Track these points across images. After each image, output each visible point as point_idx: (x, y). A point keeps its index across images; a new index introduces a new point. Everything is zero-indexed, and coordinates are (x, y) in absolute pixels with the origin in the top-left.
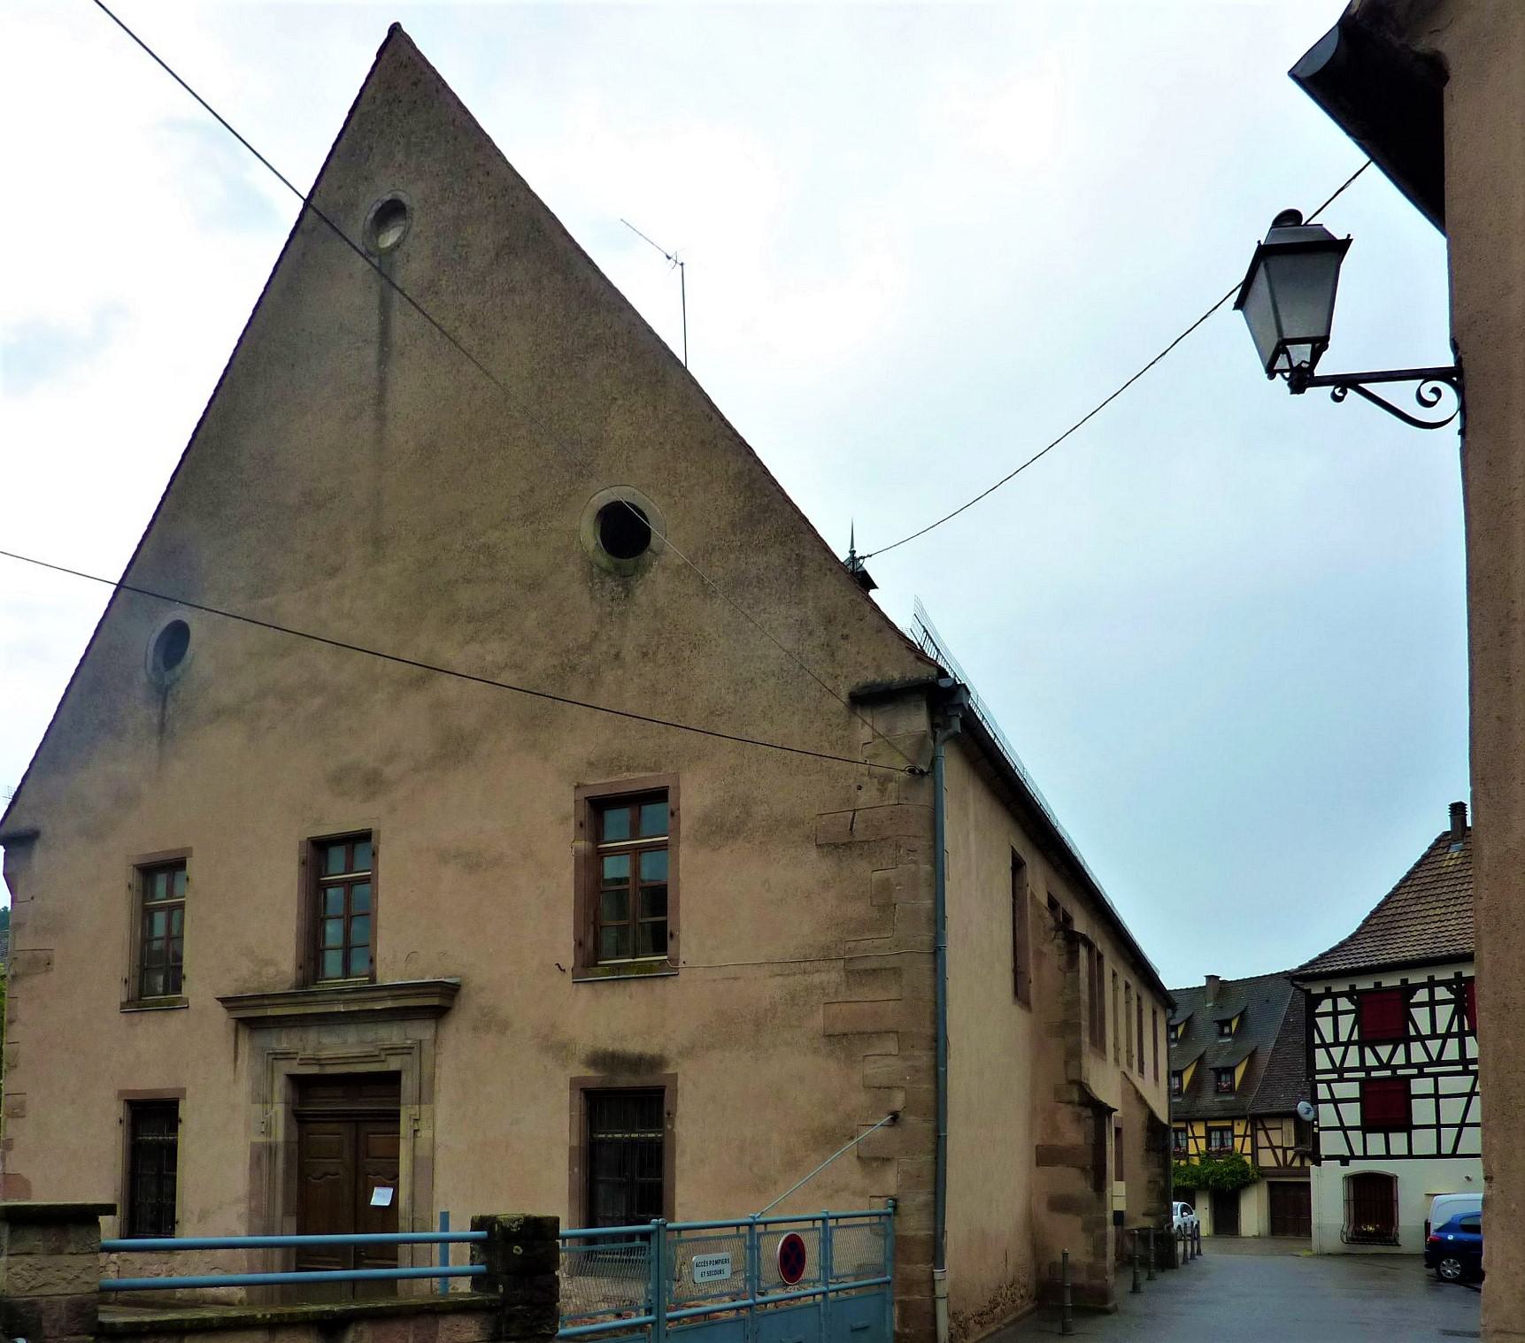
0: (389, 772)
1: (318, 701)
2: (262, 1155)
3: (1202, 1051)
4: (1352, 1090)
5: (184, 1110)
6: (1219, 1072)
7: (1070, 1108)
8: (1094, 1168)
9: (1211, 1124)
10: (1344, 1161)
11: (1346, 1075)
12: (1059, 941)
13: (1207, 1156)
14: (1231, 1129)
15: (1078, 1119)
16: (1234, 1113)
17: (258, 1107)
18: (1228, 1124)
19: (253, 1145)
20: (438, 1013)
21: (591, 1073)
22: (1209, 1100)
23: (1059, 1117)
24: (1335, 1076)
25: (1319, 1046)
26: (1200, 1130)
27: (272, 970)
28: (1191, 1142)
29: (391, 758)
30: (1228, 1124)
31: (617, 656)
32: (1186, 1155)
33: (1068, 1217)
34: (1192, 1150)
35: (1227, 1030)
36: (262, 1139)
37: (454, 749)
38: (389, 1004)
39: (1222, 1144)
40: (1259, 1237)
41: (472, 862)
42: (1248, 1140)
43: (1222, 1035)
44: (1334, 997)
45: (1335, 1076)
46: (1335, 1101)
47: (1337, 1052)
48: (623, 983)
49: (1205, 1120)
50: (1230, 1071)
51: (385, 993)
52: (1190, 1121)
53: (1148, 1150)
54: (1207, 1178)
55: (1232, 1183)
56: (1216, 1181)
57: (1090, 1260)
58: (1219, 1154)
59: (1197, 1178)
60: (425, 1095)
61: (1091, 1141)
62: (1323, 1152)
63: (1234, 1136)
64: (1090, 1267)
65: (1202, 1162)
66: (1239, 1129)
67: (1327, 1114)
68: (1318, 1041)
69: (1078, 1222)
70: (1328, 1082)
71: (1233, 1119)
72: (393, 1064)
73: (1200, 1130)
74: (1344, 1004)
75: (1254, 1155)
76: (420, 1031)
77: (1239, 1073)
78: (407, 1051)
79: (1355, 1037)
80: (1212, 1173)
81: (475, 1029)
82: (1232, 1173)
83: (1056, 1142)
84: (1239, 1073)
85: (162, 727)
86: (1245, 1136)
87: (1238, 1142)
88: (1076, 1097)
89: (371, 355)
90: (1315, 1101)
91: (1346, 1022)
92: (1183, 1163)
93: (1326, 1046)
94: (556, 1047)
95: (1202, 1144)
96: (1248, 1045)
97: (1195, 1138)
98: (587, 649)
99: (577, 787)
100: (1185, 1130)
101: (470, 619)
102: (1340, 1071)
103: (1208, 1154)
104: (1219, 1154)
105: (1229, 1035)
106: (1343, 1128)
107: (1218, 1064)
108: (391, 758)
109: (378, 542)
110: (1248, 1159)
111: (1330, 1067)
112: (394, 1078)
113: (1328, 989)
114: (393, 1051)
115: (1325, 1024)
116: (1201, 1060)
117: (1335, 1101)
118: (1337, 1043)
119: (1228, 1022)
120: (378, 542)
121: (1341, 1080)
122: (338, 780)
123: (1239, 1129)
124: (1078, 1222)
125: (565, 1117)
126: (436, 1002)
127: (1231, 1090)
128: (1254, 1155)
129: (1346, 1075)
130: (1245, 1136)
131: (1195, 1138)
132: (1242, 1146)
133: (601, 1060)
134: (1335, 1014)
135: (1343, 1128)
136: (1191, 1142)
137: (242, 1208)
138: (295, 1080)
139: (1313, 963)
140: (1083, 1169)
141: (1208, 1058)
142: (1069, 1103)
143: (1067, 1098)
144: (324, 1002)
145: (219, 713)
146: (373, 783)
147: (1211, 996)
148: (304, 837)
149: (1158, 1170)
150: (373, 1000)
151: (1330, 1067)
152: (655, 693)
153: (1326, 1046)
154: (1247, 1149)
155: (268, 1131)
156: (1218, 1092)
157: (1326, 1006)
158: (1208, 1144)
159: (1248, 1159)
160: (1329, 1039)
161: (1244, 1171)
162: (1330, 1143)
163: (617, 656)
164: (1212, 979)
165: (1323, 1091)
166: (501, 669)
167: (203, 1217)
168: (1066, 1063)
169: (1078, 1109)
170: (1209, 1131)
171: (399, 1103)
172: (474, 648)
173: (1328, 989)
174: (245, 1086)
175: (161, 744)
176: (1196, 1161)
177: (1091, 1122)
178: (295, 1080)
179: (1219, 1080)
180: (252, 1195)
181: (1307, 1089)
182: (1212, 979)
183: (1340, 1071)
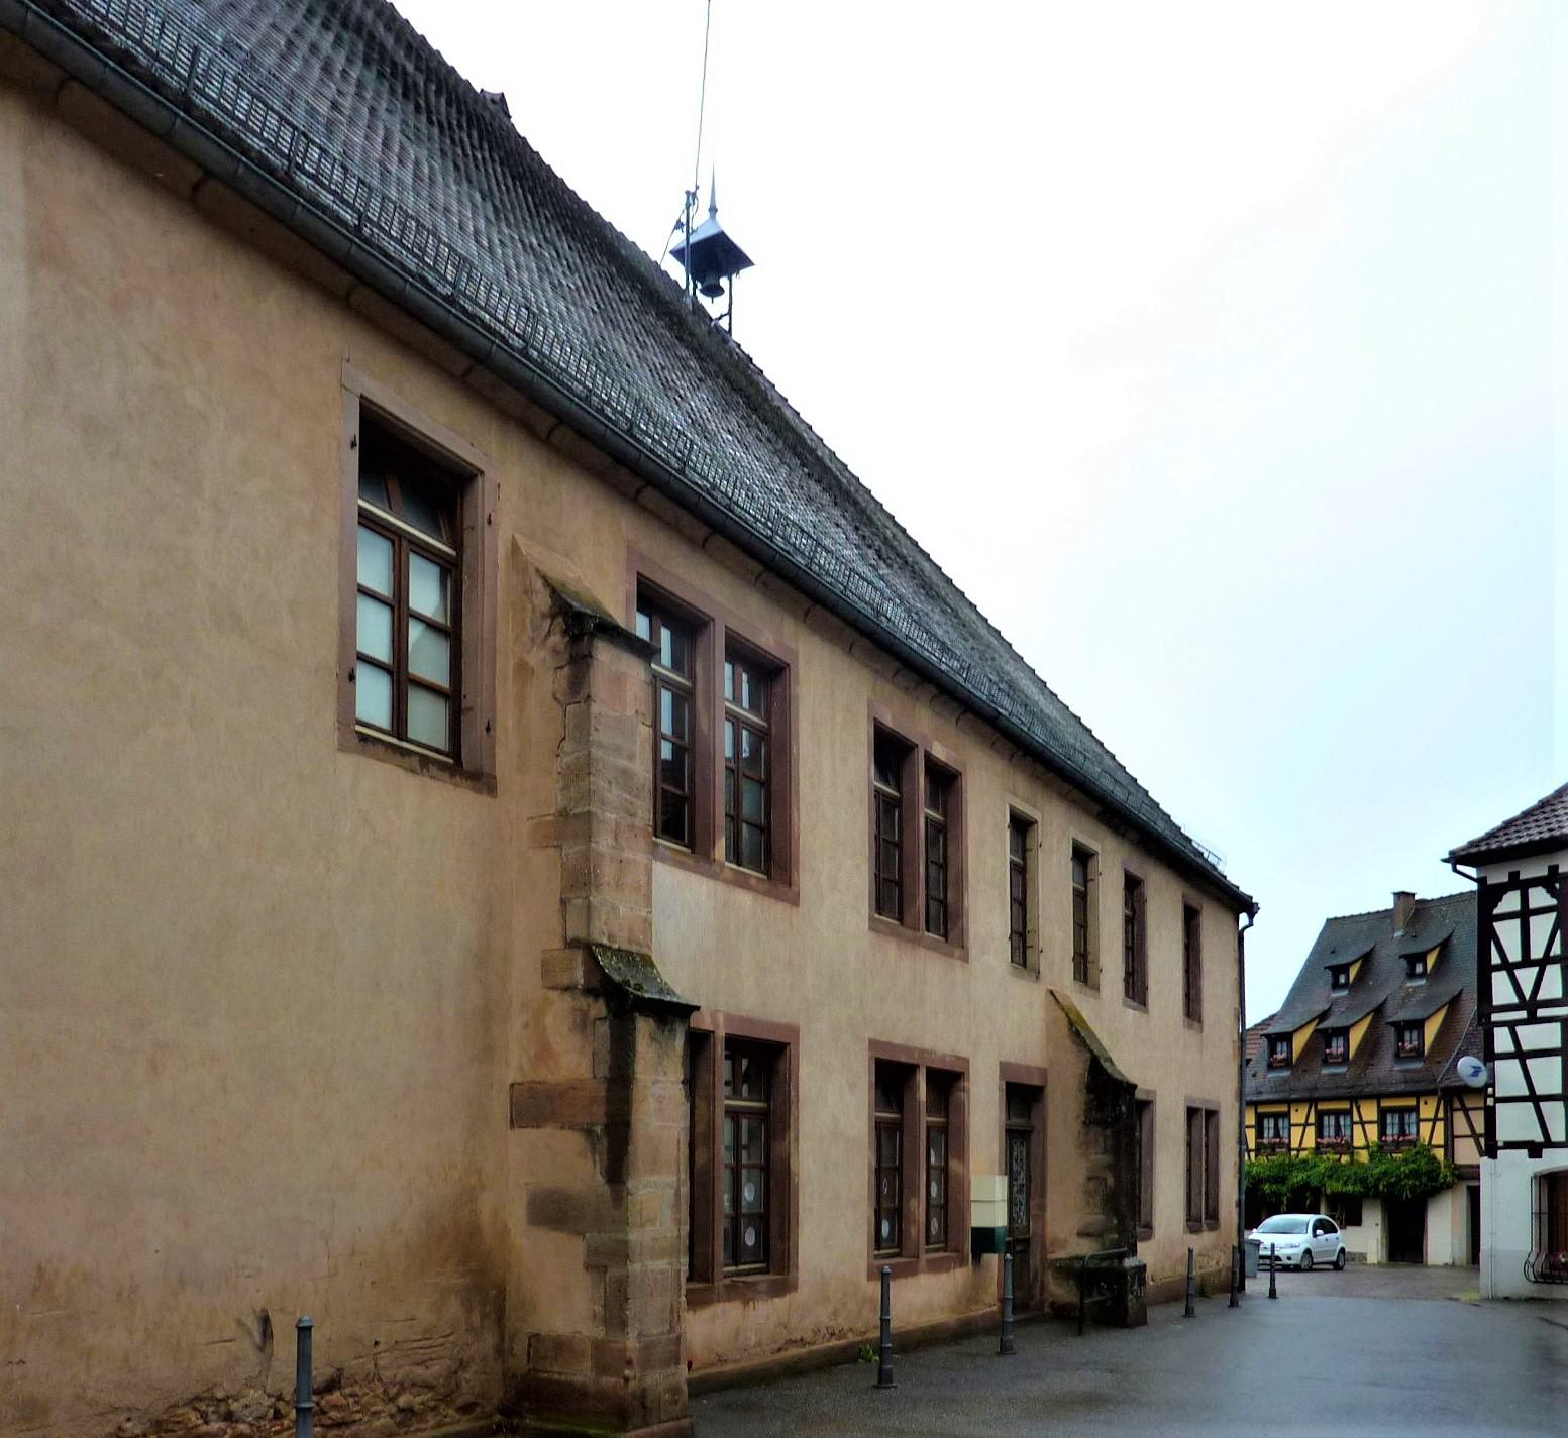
3: (1381, 1000)
4: (1550, 1036)
6: (1402, 1028)
7: (567, 997)
8: (608, 1128)
9: (1386, 1103)
10: (1535, 1150)
11: (1541, 1013)
12: (556, 639)
13: (1381, 1150)
14: (1416, 1109)
15: (583, 1024)
16: (1419, 1087)
18: (1411, 1102)
22: (1387, 1069)
23: (549, 1020)
24: (1523, 1015)
25: (1498, 968)
26: (1370, 1111)
28: (1358, 1129)
30: (1411, 1102)
32: (1349, 1148)
33: (558, 1238)
34: (1359, 1141)
35: (1419, 968)
39: (1403, 1132)
40: (1453, 1266)
42: (1440, 1126)
43: (1412, 975)
44: (1524, 886)
45: (1523, 1015)
46: (1521, 1055)
47: (1526, 977)
49: (1378, 1097)
50: (1418, 1025)
52: (1356, 1098)
53: (1087, 1124)
54: (1379, 1180)
55: (1413, 1188)
56: (1389, 1185)
57: (600, 1333)
58: (1398, 1145)
59: (1363, 1180)
61: (603, 1070)
62: (1502, 1136)
63: (1418, 1121)
64: (598, 1347)
65: (1372, 1157)
66: (1427, 1110)
67: (1509, 1078)
68: (1496, 959)
69: (577, 1248)
70: (1512, 1026)
71: (1417, 1095)
73: (1370, 1111)
74: (1539, 897)
75: (1449, 1146)
77: (1431, 1030)
79: (1556, 949)
80: (1385, 1173)
82: (1414, 1174)
83: (544, 1074)
84: (1431, 1030)
86: (1435, 1120)
87: (1425, 1128)
88: (579, 976)
90: (1490, 1056)
91: (1542, 926)
92: (1345, 1159)
93: (1509, 967)
95: (1373, 1131)
96: (1449, 988)
97: (1363, 1123)
100: (1349, 1113)
102: (1531, 1007)
103: (1382, 1147)
104: (1398, 1145)
105: (1423, 974)
106: (1534, 1098)
107: (1402, 1016)
110: (1439, 1154)
111: (1515, 1000)
113: (1514, 875)
115: (1508, 933)
116: (1379, 1011)
117: (1521, 1055)
118: (1526, 961)
119: (1421, 957)
121: (1532, 1020)
123: (1427, 1110)
124: (577, 1248)
127: (1418, 1053)
128: (1449, 1146)
129: (1541, 1013)
130: (1435, 1120)
131: (1363, 1123)
132: (1430, 1134)
134: (1525, 914)
135: (1534, 1098)
136: (1358, 1129)
139: (1492, 835)
140: (588, 1133)
141: (1390, 1008)
142: (567, 989)
143: (565, 981)
147: (1400, 920)
149: (1106, 1159)
151: (1515, 1000)
153: (1509, 967)
154: (1439, 1138)
156: (1398, 1056)
157: (1511, 902)
158: (1382, 1132)
159: (1439, 1154)
160: (1514, 955)
161: (1432, 1172)
162: (1514, 1122)
164: (1403, 896)
165: (1502, 1041)
168: (564, 902)
169: (584, 1002)
170: (1383, 1113)
173: (1514, 875)
176: (1364, 1157)
177: (604, 1029)
179: (1401, 1038)
181: (1480, 1041)
182: (1403, 896)
183: (1531, 1007)
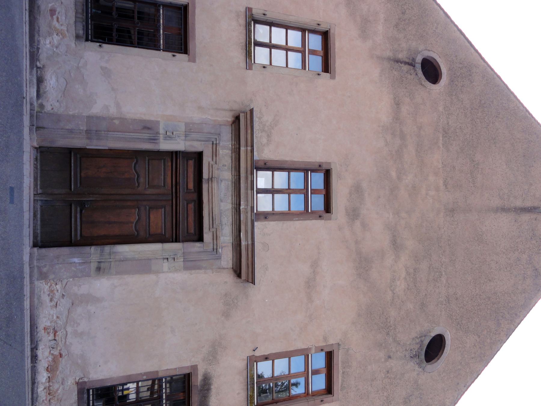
0: (358, 224)
1: (394, 174)
2: (148, 127)
5: (181, 57)
17: (183, 128)
19: (158, 122)
20: (238, 273)
21: (200, 378)
27: (264, 141)
29: (364, 226)
31: (390, 357)
36: (162, 131)
37: (363, 264)
38: (243, 243)
41: (310, 284)
48: (246, 387)
51: (250, 242)
60: (191, 265)
72: (207, 236)
76: (227, 257)
78: (215, 250)
81: (226, 295)
85: (398, 61)
89: (519, 203)
94: (214, 352)
98: (395, 340)
99: (339, 344)
101: (415, 270)
108: (364, 226)
109: (452, 211)
112: (200, 239)
114: (215, 237)
120: (452, 211)
122: (357, 190)
125: (173, 366)
126: (243, 269)
133: (207, 382)
137: (113, 111)
138: (199, 156)
144: (247, 178)
145: (397, 104)
146: (354, 214)
148: (333, 167)
150: (246, 232)
152: (372, 380)
155: (167, 137)
163: (390, 357)
166: (392, 291)
167: (106, 73)
171: (183, 241)
172: (404, 274)
174: (196, 116)
175: (389, 59)
178: (199, 156)
180: (122, 120)
